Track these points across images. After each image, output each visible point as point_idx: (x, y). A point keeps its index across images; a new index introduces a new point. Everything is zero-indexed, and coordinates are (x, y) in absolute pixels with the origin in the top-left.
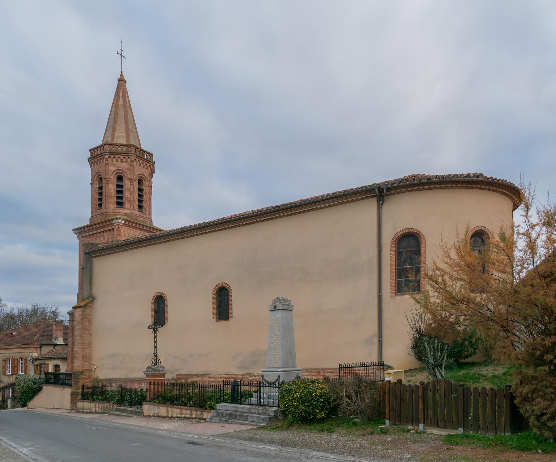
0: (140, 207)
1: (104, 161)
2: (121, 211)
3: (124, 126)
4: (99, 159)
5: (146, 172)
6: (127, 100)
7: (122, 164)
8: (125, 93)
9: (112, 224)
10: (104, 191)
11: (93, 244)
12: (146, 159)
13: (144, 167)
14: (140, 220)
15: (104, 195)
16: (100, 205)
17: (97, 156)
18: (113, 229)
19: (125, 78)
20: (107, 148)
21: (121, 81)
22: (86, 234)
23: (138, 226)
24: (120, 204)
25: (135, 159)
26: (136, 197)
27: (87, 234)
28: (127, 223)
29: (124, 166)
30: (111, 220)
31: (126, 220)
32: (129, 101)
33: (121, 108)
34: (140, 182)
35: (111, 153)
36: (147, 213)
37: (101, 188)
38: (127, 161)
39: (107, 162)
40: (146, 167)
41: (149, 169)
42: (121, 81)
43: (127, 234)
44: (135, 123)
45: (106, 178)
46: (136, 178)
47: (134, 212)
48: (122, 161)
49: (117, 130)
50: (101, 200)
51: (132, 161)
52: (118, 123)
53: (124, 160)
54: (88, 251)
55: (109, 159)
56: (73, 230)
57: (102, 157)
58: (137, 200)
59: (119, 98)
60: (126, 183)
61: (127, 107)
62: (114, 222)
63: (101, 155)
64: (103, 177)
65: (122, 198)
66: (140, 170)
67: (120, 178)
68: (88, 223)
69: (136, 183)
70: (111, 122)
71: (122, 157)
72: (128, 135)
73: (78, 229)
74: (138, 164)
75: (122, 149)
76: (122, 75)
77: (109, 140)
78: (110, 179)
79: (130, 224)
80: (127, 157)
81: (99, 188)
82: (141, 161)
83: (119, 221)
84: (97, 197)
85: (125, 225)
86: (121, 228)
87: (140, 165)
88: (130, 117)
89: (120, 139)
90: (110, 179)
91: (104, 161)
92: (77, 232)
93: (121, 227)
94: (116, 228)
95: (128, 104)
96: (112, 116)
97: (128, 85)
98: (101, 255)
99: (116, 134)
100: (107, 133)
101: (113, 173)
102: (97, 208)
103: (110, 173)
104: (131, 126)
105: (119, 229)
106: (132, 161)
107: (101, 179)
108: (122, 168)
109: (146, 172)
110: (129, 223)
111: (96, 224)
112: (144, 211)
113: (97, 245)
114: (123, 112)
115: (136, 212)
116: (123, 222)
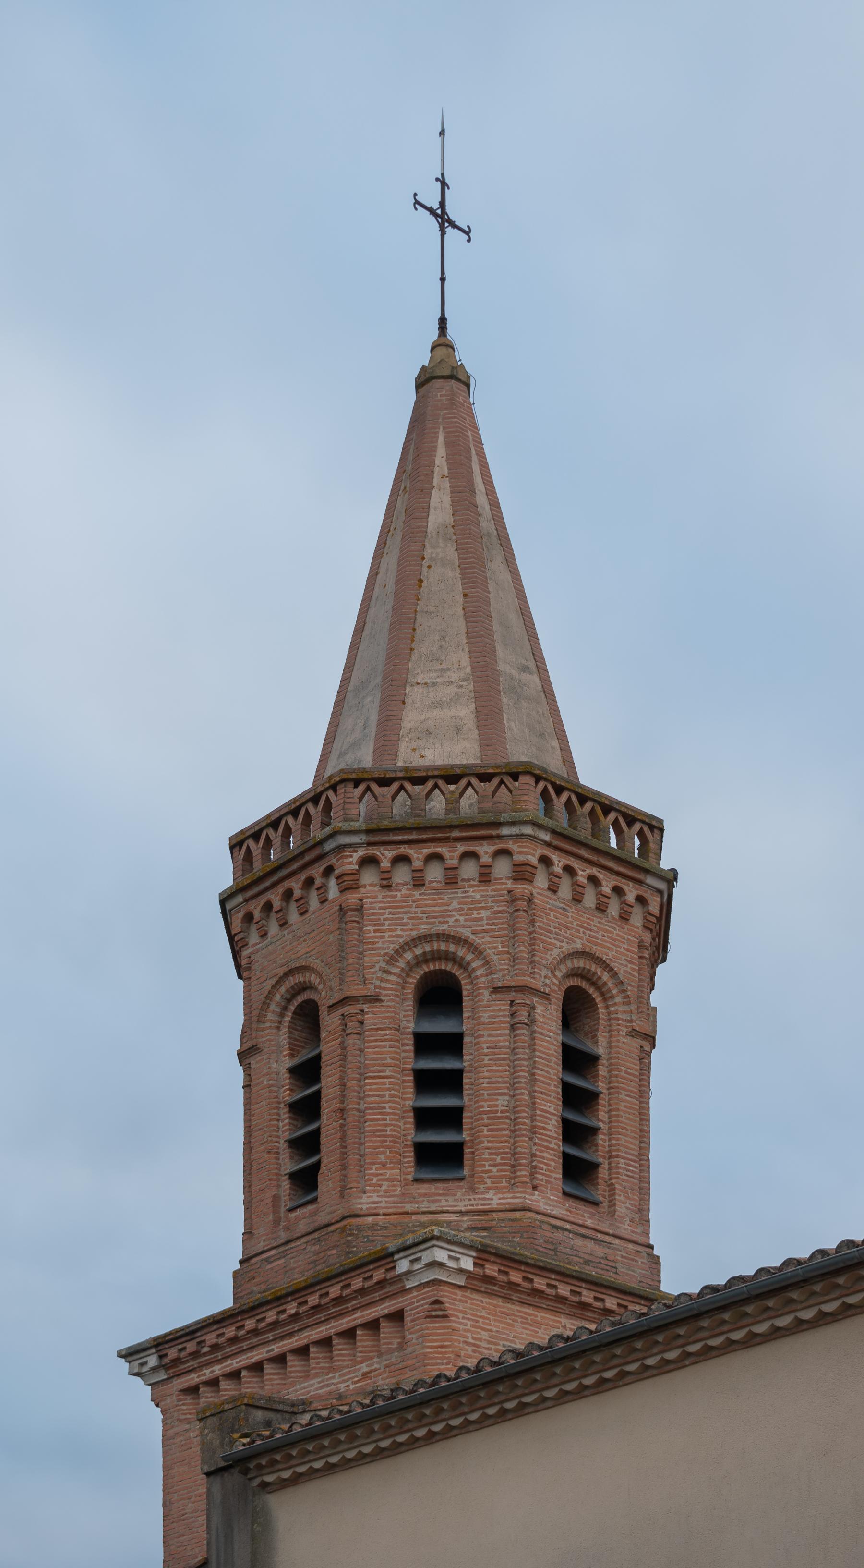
0: (578, 1172)
1: (333, 891)
2: (445, 1203)
3: (460, 659)
4: (296, 885)
5: (618, 943)
6: (481, 499)
7: (453, 899)
8: (466, 449)
9: (393, 1285)
10: (329, 1083)
11: (271, 1406)
12: (615, 852)
13: (601, 908)
14: (580, 1252)
15: (327, 1107)
16: (306, 1181)
17: (277, 868)
18: (397, 1317)
19: (466, 355)
20: (358, 808)
21: (442, 381)
22: (208, 1373)
23: (564, 1290)
24: (440, 1156)
25: (545, 861)
26: (551, 1109)
27: (217, 1370)
28: (491, 1270)
29: (467, 910)
30: (386, 1257)
31: (483, 1253)
32: (495, 505)
33: (442, 554)
34: (576, 1007)
35: (378, 833)
36: (621, 1209)
37: (308, 1072)
38: (485, 877)
39: (352, 898)
40: (614, 909)
41: (637, 919)
42: (442, 381)
43: (489, 1330)
44: (533, 637)
45: (346, 1000)
46: (552, 982)
47: (535, 1200)
48: (452, 880)
49: (415, 695)
50: (307, 1145)
51: (522, 873)
52: (423, 648)
53: (469, 870)
54: (240, 1445)
55: (369, 877)
56: (129, 1354)
57: (316, 871)
58: (553, 1128)
59: (427, 491)
60: (484, 1021)
61: (482, 540)
62: (403, 1266)
63: (314, 854)
64: (324, 998)
65: (453, 1118)
66: (572, 926)
67: (440, 994)
68: (225, 1301)
69: (548, 1016)
70: (375, 652)
71: (451, 853)
72: (488, 716)
73: (159, 1344)
74: (565, 890)
75: (453, 804)
76: (443, 343)
77: (365, 758)
78: (375, 999)
79: (516, 1277)
80: (485, 850)
81: (292, 1071)
82: (583, 873)
83: (441, 1255)
84: (285, 1128)
85: (478, 1282)
86: (454, 1301)
87: (577, 899)
88: (500, 602)
89: (440, 732)
90: (375, 999)
91: (333, 891)
92: (152, 1361)
93: (448, 1296)
94: (414, 1304)
95: (486, 524)
96: (382, 612)
97: (488, 407)
98: (330, 1469)
99: (410, 719)
100: (347, 723)
101: (391, 960)
102: (286, 1201)
103: (375, 961)
104: (507, 662)
105: (437, 1311)
106: (522, 873)
107: (308, 1017)
108: (458, 922)
109: (618, 943)
110: (506, 1268)
111: (278, 1300)
112: (600, 1193)
113: (294, 1409)
114: (453, 575)
115: (549, 1199)
116: (467, 1264)
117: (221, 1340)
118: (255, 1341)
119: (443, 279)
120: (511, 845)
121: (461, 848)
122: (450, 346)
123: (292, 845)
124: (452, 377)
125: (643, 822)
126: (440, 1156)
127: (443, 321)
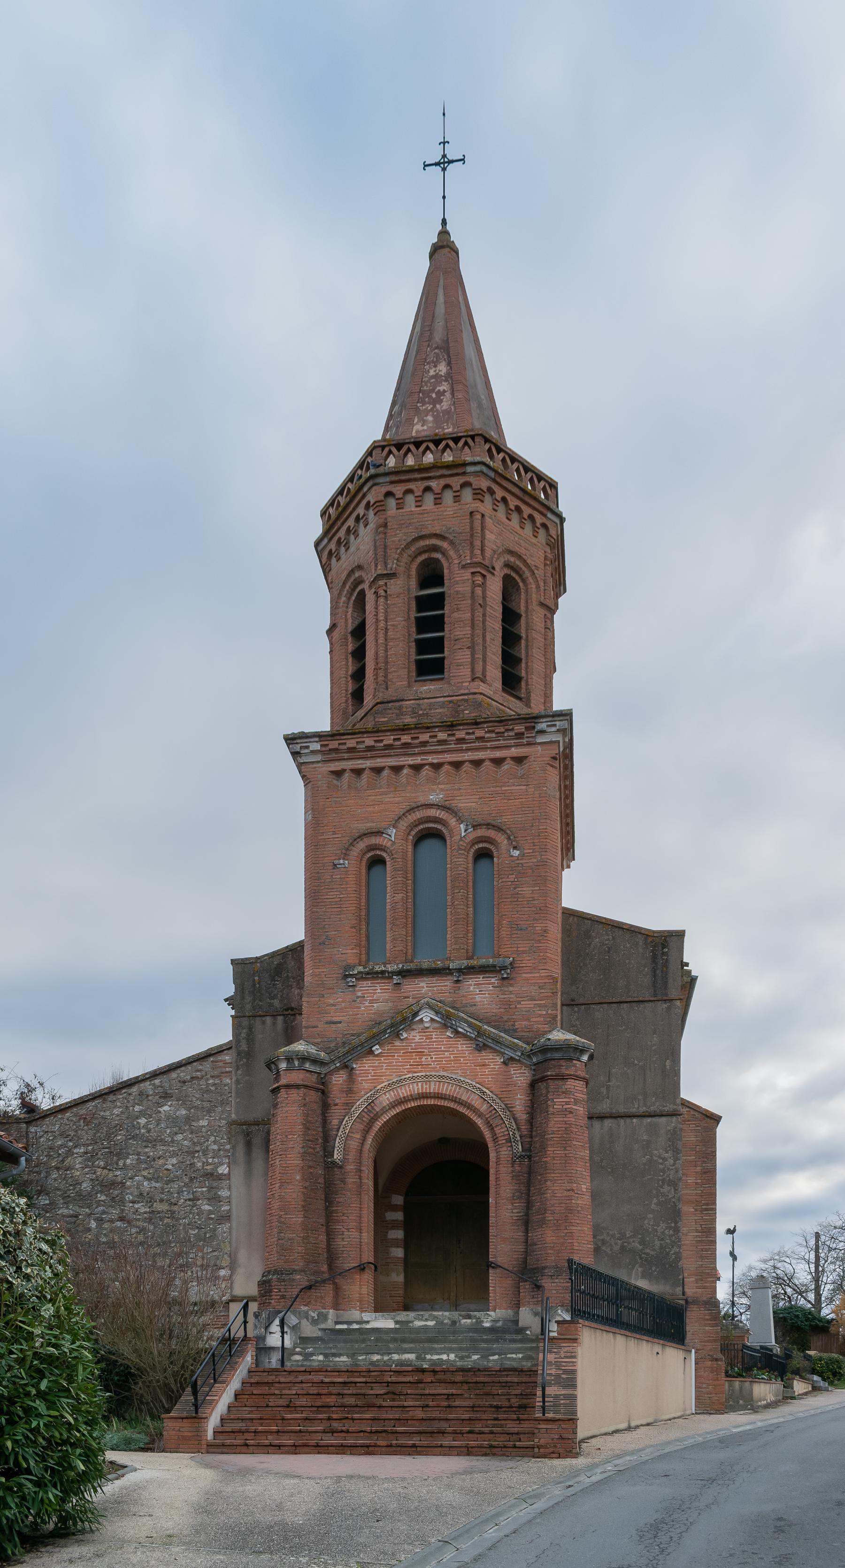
12: (532, 496)
21: (444, 251)
42: (444, 251)
76: (444, 233)
117: (341, 747)
118: (334, 755)
119: (444, 197)
120: (471, 479)
121: (443, 482)
122: (447, 233)
123: (389, 946)
124: (448, 246)
125: (546, 481)
126: (430, 663)
127: (444, 222)
